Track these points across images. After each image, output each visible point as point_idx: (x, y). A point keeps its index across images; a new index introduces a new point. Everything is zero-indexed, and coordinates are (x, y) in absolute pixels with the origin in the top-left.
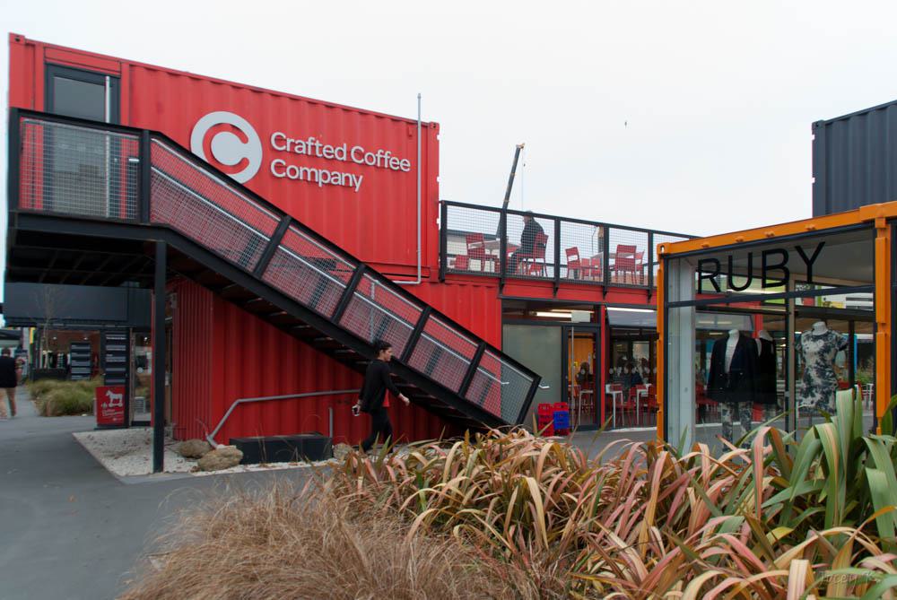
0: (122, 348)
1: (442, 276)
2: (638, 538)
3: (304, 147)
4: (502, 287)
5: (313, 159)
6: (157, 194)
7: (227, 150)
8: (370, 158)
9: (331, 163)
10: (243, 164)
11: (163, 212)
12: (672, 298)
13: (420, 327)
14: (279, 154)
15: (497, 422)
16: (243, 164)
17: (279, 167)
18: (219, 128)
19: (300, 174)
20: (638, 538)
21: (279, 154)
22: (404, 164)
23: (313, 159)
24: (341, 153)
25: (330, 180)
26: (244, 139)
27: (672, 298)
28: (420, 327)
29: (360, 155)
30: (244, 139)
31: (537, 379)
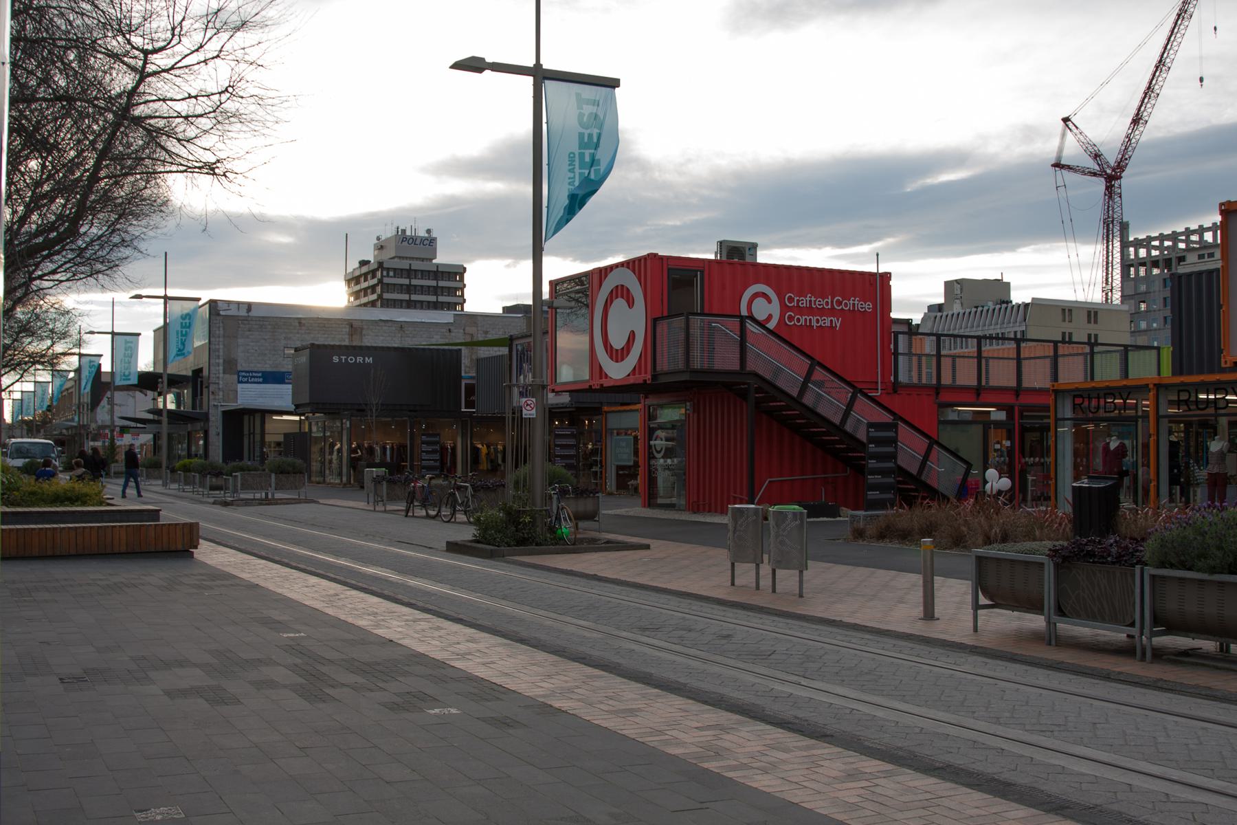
0: (572, 442)
1: (896, 387)
2: (484, 720)
3: (805, 302)
4: (938, 394)
5: (810, 310)
6: (750, 356)
7: (761, 310)
8: (846, 305)
9: (822, 312)
10: (770, 317)
11: (751, 366)
12: (1059, 416)
13: (850, 406)
14: (790, 309)
15: (933, 494)
16: (770, 317)
17: (791, 318)
18: (756, 295)
19: (802, 321)
20: (484, 720)
21: (790, 309)
22: (868, 306)
23: (810, 310)
24: (827, 303)
25: (821, 323)
26: (770, 301)
27: (1059, 416)
28: (850, 406)
29: (839, 303)
30: (770, 301)
31: (969, 466)
